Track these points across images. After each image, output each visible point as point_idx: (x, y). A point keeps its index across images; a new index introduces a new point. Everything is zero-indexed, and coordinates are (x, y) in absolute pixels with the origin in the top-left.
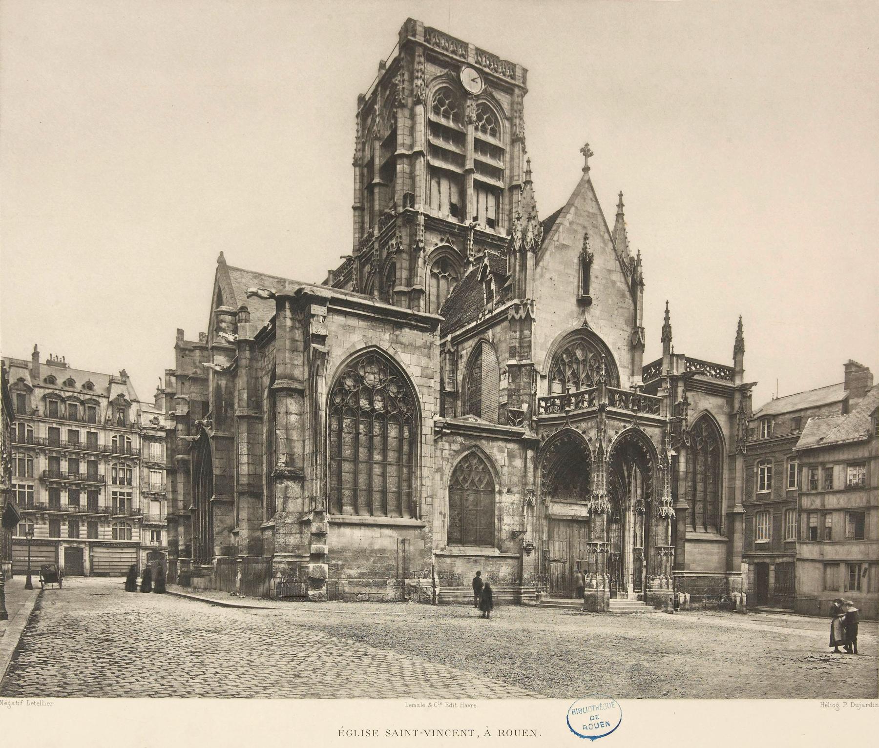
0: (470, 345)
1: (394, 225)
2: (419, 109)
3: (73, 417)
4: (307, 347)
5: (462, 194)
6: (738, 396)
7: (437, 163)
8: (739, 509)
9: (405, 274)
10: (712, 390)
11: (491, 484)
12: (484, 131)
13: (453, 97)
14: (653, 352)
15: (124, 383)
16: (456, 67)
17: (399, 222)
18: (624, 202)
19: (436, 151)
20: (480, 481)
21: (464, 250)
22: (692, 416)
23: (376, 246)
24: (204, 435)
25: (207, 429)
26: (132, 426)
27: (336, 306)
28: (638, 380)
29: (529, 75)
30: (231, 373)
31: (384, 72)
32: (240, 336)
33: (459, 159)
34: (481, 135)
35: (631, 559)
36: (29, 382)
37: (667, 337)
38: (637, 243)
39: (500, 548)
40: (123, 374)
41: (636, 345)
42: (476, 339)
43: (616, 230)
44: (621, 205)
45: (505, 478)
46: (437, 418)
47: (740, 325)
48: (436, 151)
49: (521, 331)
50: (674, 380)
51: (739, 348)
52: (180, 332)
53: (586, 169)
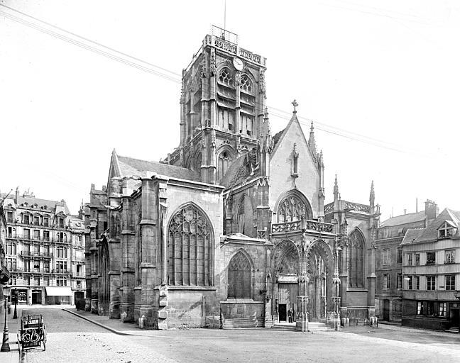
0: (238, 196)
1: (201, 134)
2: (213, 79)
3: (37, 224)
4: (157, 204)
5: (234, 119)
6: (372, 219)
7: (220, 104)
8: (373, 275)
9: (206, 159)
10: (358, 217)
11: (249, 267)
12: (245, 88)
13: (228, 73)
14: (329, 198)
15: (63, 206)
16: (232, 59)
17: (203, 134)
18: (314, 126)
19: (220, 98)
20: (244, 266)
21: (236, 147)
22: (349, 230)
23: (192, 144)
24: (105, 240)
25: (107, 238)
26: (67, 228)
27: (173, 183)
28: (322, 214)
29: (267, 61)
30: (119, 210)
31: (195, 59)
32: (124, 195)
33: (233, 102)
34: (243, 91)
35: (320, 302)
36: (14, 206)
37: (336, 193)
38: (320, 146)
39: (253, 299)
40: (63, 201)
41: (321, 196)
42: (242, 193)
43: (310, 141)
44: (312, 128)
45: (256, 264)
46: (222, 236)
47: (372, 185)
48: (220, 98)
49: (264, 191)
50: (339, 212)
51: (372, 198)
52: (93, 186)
53: (295, 112)
